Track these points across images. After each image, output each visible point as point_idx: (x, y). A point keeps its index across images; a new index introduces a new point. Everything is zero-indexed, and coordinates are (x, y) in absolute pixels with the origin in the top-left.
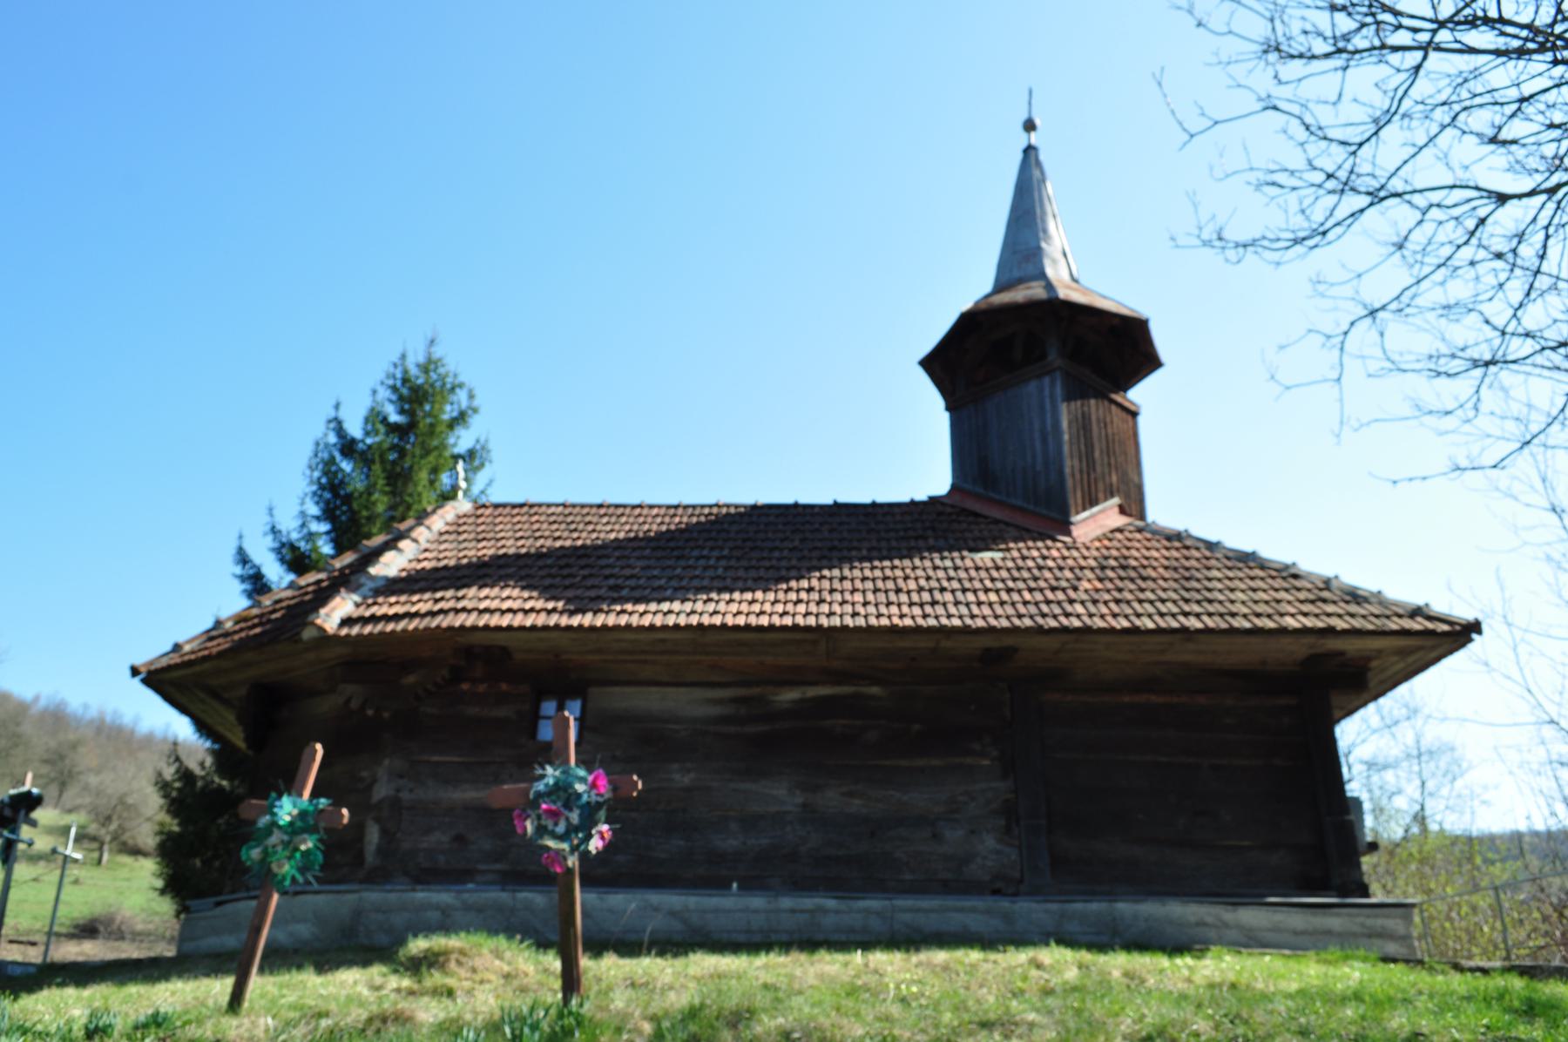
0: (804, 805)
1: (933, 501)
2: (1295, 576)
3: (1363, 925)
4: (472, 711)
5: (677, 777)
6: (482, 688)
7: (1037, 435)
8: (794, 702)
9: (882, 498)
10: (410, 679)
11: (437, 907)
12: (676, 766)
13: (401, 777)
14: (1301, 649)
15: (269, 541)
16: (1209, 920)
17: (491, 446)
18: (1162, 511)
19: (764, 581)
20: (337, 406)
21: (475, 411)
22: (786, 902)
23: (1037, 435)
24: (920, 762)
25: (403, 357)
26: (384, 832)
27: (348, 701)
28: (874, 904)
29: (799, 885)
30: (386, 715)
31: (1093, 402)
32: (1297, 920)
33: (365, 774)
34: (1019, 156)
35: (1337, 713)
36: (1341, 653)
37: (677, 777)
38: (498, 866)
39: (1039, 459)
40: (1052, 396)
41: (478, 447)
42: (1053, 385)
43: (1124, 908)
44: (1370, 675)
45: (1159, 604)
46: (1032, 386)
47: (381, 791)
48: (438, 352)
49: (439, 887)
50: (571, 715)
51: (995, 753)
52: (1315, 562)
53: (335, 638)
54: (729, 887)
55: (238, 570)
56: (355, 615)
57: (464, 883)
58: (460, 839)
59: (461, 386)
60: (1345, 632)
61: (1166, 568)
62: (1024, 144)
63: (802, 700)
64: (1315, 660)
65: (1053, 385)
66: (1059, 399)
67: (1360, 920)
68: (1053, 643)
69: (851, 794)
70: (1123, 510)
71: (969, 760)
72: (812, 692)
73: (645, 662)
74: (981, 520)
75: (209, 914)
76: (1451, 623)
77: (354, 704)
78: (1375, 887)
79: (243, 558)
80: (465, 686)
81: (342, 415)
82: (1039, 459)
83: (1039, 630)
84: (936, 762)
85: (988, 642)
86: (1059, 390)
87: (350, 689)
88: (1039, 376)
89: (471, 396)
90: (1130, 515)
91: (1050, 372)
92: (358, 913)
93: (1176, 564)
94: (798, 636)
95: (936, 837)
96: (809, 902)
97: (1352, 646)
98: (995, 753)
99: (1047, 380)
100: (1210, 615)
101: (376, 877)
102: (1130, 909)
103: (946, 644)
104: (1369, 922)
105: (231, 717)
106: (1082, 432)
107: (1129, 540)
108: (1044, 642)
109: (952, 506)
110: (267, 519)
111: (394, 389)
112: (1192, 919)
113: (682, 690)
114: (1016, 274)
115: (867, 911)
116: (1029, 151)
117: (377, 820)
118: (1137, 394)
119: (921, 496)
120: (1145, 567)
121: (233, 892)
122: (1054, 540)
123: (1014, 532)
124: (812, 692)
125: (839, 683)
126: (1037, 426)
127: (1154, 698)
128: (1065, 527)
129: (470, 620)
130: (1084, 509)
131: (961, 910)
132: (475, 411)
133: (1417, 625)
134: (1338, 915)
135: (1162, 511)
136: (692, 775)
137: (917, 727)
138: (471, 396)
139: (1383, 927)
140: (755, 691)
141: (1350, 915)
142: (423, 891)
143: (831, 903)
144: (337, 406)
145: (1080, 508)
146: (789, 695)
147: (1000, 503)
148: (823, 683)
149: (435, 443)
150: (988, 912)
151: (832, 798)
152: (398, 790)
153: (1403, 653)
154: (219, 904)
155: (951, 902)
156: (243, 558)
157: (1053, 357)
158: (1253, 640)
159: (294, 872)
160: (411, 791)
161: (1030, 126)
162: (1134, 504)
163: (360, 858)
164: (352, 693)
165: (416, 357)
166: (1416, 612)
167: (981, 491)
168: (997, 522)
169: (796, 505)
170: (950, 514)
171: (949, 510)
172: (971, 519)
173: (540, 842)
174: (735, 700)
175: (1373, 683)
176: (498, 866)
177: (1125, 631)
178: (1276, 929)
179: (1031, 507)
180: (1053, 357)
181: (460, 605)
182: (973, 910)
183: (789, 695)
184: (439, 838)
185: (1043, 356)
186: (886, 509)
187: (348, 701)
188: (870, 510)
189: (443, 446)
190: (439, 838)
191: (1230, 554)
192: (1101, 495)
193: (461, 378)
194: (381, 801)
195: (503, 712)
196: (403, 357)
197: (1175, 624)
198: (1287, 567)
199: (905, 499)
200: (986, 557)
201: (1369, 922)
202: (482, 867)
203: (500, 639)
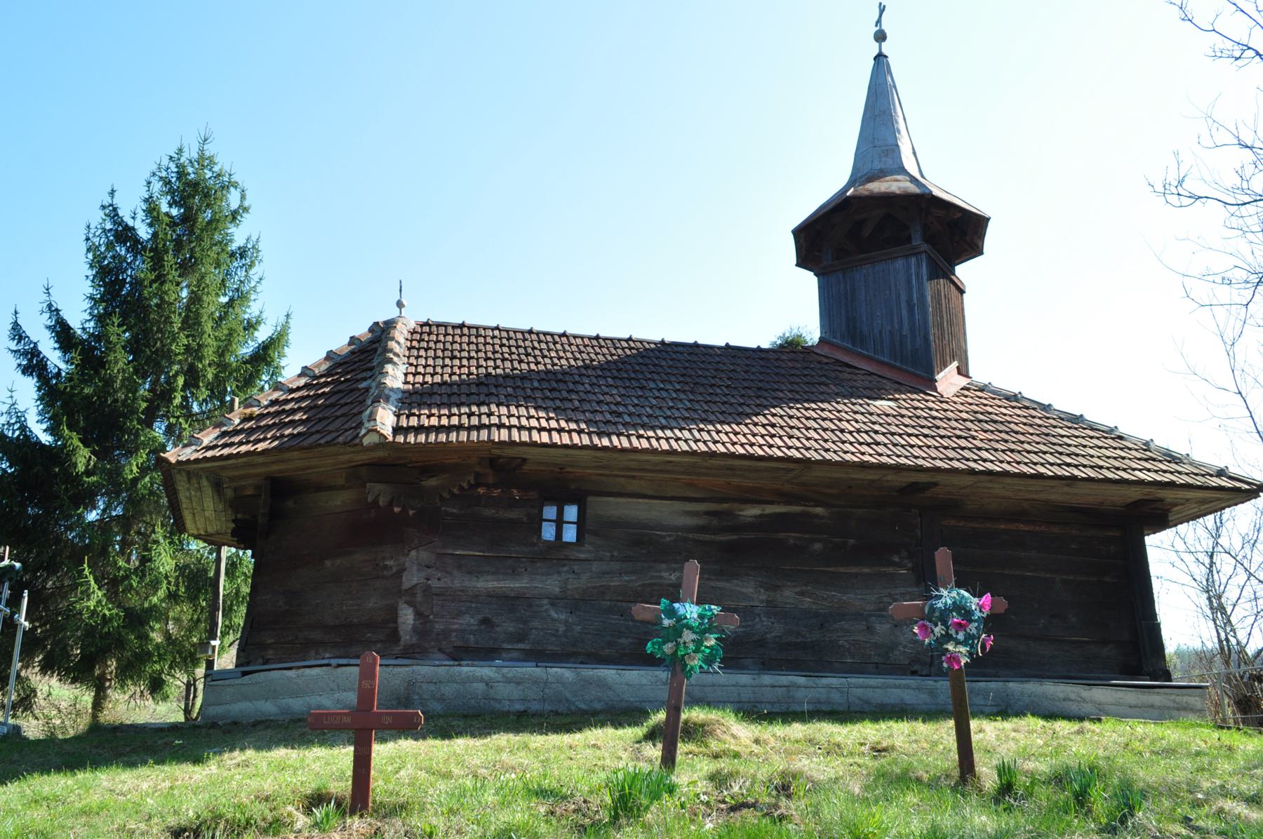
2: (1121, 438)
3: (1174, 701)
4: (488, 512)
5: (665, 575)
6: (496, 492)
8: (755, 517)
10: (433, 482)
11: (481, 680)
14: (1135, 494)
15: (46, 319)
16: (1073, 696)
17: (261, 246)
18: (980, 372)
19: (738, 415)
20: (112, 193)
21: (246, 210)
22: (767, 679)
23: (904, 305)
24: (854, 570)
25: (180, 151)
26: (418, 614)
28: (834, 681)
29: (768, 665)
30: (411, 512)
31: (942, 280)
32: (1131, 697)
34: (871, 63)
36: (1161, 500)
37: (665, 575)
38: (521, 646)
40: (918, 275)
41: (249, 246)
42: (919, 266)
43: (1014, 686)
46: (900, 263)
47: (412, 578)
48: (210, 150)
49: (482, 663)
50: (571, 512)
51: (910, 565)
52: (1135, 427)
55: (13, 345)
57: (493, 659)
58: (485, 621)
59: (235, 185)
60: (1182, 485)
62: (876, 52)
63: (761, 516)
65: (919, 266)
66: (925, 278)
67: (1173, 697)
69: (802, 594)
71: (891, 570)
73: (633, 477)
75: (237, 681)
76: (1248, 483)
77: (382, 502)
78: (1175, 675)
79: (17, 333)
80: (481, 491)
81: (117, 201)
84: (866, 570)
86: (924, 270)
87: (378, 487)
88: (906, 256)
89: (243, 197)
92: (411, 684)
95: (870, 629)
96: (785, 679)
97: (1168, 495)
98: (910, 565)
99: (913, 260)
101: (413, 653)
102: (1033, 688)
104: (1178, 699)
108: (956, 480)
110: (45, 297)
111: (167, 182)
112: (1061, 695)
114: (878, 166)
115: (829, 687)
116: (880, 58)
117: (411, 604)
123: (888, 385)
125: (789, 503)
126: (904, 297)
127: (1022, 527)
131: (896, 687)
132: (246, 210)
133: (1216, 482)
135: (980, 372)
137: (852, 541)
138: (243, 197)
140: (726, 506)
142: (468, 665)
143: (802, 680)
144: (112, 193)
146: (752, 511)
147: (869, 359)
148: (779, 503)
149: (217, 237)
150: (918, 689)
151: (788, 595)
153: (1203, 502)
155: (891, 681)
156: (17, 333)
157: (917, 241)
158: (1104, 487)
159: (701, 663)
160: (439, 579)
161: (880, 37)
162: (963, 371)
163: (394, 636)
165: (192, 153)
166: (1221, 473)
167: (850, 346)
169: (696, 345)
173: (945, 646)
174: (708, 513)
176: (521, 646)
178: (1117, 704)
179: (898, 364)
180: (917, 241)
182: (907, 687)
183: (752, 511)
184: (469, 621)
189: (223, 244)
190: (469, 621)
191: (1062, 416)
193: (234, 178)
195: (513, 514)
196: (180, 151)
198: (1111, 430)
199: (691, 341)
200: (883, 405)
201: (1178, 699)
202: (506, 646)
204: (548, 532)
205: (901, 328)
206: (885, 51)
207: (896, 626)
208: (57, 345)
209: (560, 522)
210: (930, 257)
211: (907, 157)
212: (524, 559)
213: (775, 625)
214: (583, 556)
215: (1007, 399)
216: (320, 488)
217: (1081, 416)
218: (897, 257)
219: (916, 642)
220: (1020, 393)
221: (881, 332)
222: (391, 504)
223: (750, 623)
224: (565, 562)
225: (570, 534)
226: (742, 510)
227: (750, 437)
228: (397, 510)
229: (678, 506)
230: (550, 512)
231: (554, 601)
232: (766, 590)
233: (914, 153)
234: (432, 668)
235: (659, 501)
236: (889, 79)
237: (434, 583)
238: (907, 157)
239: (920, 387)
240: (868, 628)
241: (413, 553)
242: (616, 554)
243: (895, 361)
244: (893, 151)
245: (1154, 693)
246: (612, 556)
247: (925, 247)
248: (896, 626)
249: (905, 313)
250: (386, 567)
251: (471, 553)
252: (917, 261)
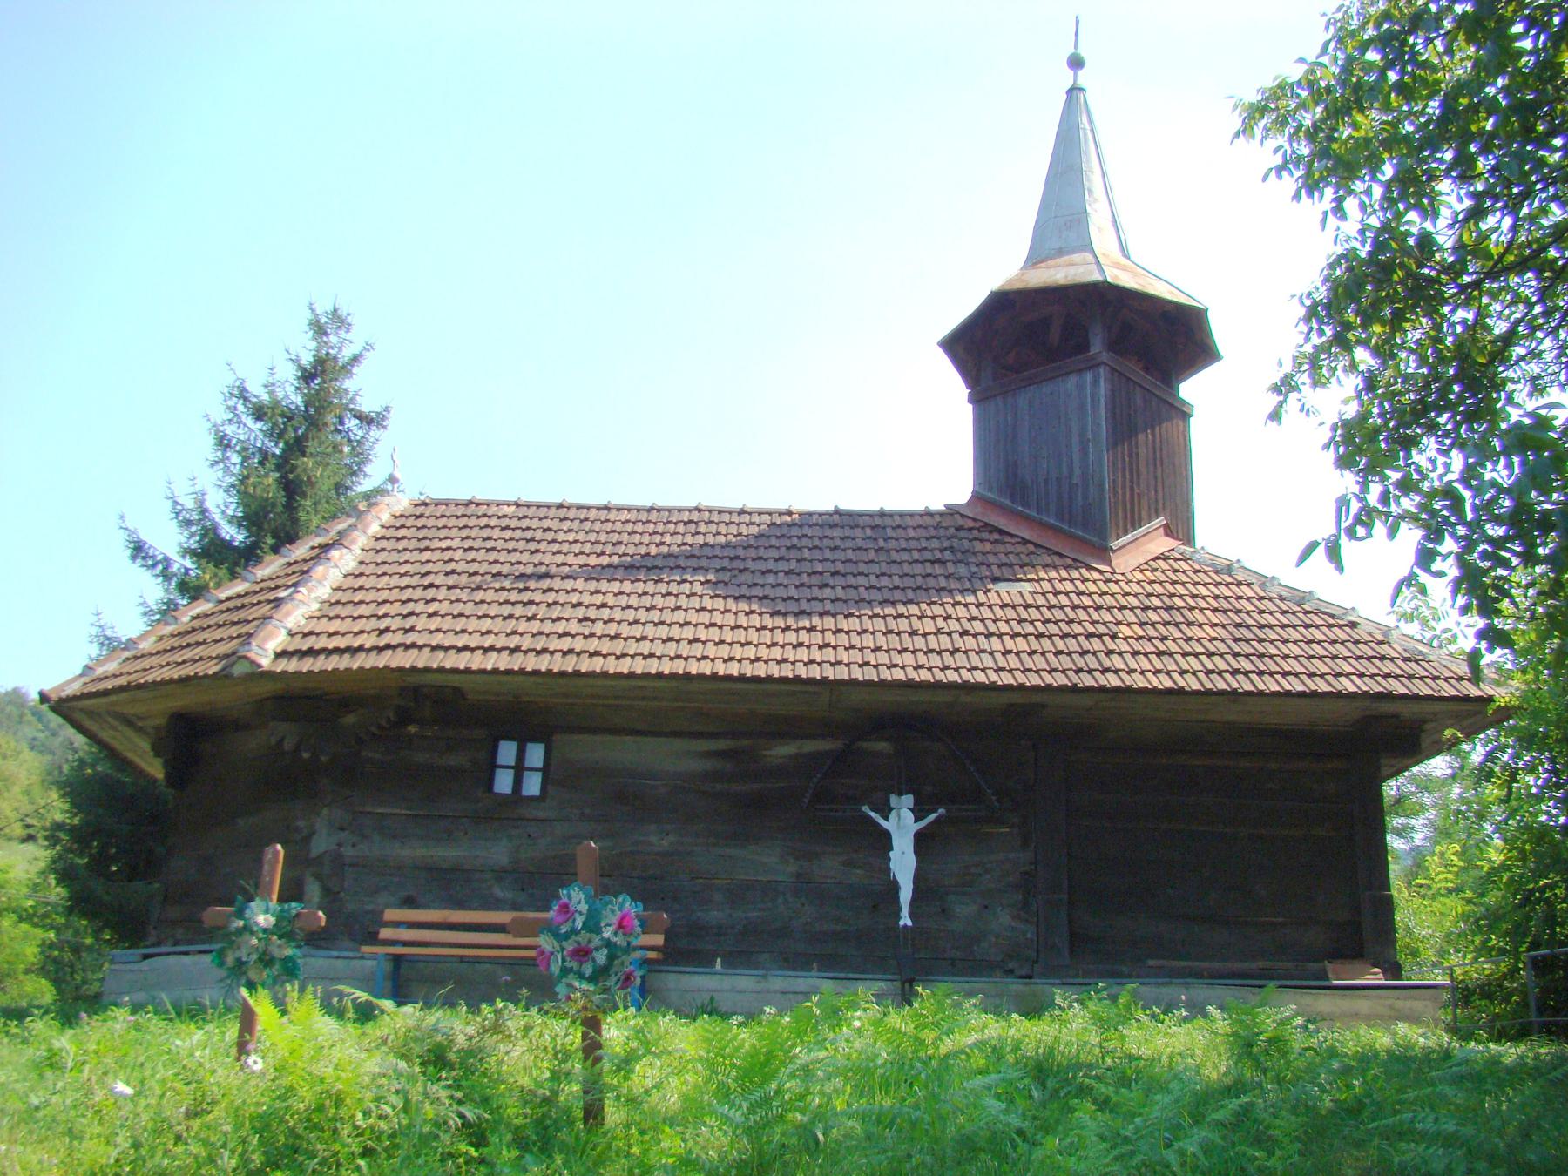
0: (799, 875)
1: (951, 511)
4: (420, 757)
7: (1075, 440)
8: (790, 757)
9: (892, 506)
10: (350, 719)
12: (653, 827)
13: (342, 829)
23: (1075, 440)
27: (281, 741)
33: (301, 824)
35: (1385, 771)
37: (654, 839)
39: (1077, 471)
42: (1095, 382)
44: (1423, 735)
45: (1186, 612)
46: (1072, 381)
47: (322, 844)
50: (536, 754)
53: (269, 675)
54: (712, 963)
56: (291, 649)
61: (1215, 610)
62: (1081, 73)
63: (798, 756)
64: (1368, 721)
65: (1095, 382)
68: (1085, 701)
69: (850, 864)
70: (1169, 531)
72: (810, 746)
74: (1008, 539)
77: (288, 745)
80: (412, 729)
82: (1077, 471)
83: (1074, 689)
85: (1016, 698)
87: (284, 727)
90: (1177, 539)
91: (1093, 366)
93: (1226, 605)
94: (798, 688)
99: (1089, 376)
100: (1261, 673)
103: (966, 699)
105: (145, 745)
106: (1050, 263)
107: (1175, 571)
109: (974, 520)
113: (662, 739)
116: (1074, 91)
117: (318, 877)
118: (1190, 389)
119: (938, 505)
120: (1191, 609)
121: (159, 944)
122: (1089, 568)
124: (810, 746)
128: (1103, 553)
129: (422, 660)
130: (1126, 533)
134: (1367, 997)
136: (672, 838)
139: (1411, 1009)
141: (1380, 997)
145: (1120, 532)
146: (783, 751)
147: (1028, 519)
148: (823, 737)
152: (340, 845)
154: (146, 957)
160: (354, 845)
162: (1181, 528)
164: (287, 733)
168: (1025, 542)
170: (970, 529)
171: (971, 524)
172: (996, 536)
175: (1426, 742)
177: (1169, 691)
179: (1065, 527)
180: (1097, 346)
181: (410, 638)
183: (783, 751)
185: (1084, 347)
186: (898, 520)
187: (281, 741)
188: (878, 521)
191: (1284, 594)
192: (1144, 514)
194: (321, 856)
197: (1222, 686)
201: (1399, 1004)
203: (455, 680)
204: (504, 782)
205: (1070, 477)
206: (1081, 83)
207: (986, 907)
208: (58, 809)
209: (520, 769)
210: (1113, 369)
211: (1100, 229)
212: (464, 820)
213: (806, 907)
214: (541, 814)
215: (1217, 572)
216: (238, 726)
217: (1311, 593)
218: (1068, 374)
219: (1514, 1012)
220: (1238, 561)
221: (1046, 481)
222: (297, 749)
223: (770, 905)
224: (519, 822)
225: (533, 785)
226: (770, 749)
227: (1168, 585)
228: (305, 755)
229: (679, 744)
230: (507, 752)
231: (500, 874)
232: (797, 859)
233: (1115, 222)
234: (327, 961)
235: (611, 738)
236: (1085, 119)
237: (348, 851)
238: (1100, 229)
239: (1081, 558)
240: (943, 911)
241: (325, 811)
242: (587, 811)
243: (1062, 520)
244: (1079, 221)
245: (1359, 997)
246: (582, 814)
247: (1105, 357)
248: (986, 907)
249: (1076, 449)
250: (297, 830)
251: (397, 811)
252: (1094, 377)
